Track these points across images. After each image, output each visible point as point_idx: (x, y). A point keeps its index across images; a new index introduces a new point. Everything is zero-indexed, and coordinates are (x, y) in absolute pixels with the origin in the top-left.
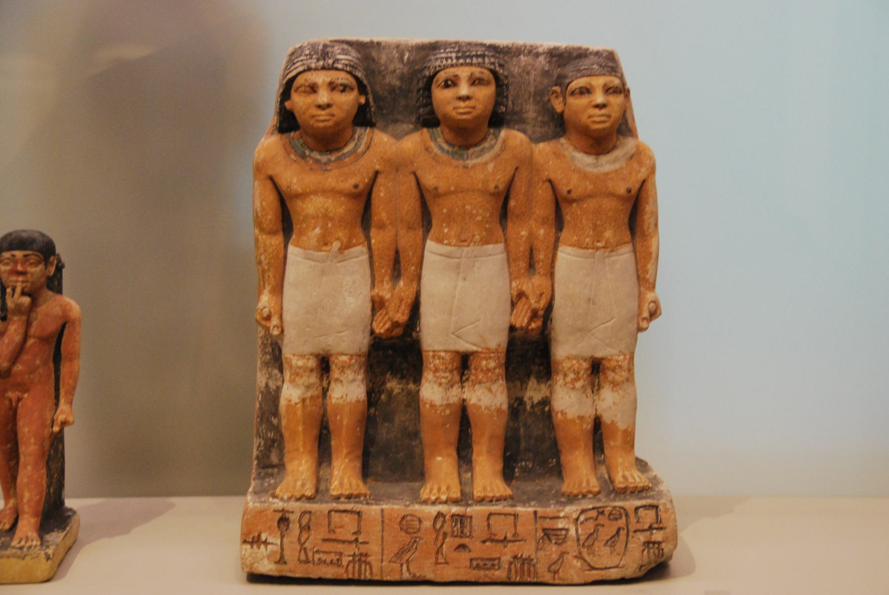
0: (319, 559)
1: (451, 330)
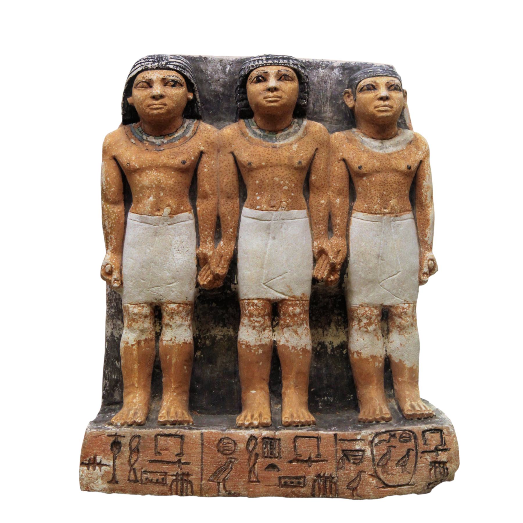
0: (146, 479)
1: (263, 281)
